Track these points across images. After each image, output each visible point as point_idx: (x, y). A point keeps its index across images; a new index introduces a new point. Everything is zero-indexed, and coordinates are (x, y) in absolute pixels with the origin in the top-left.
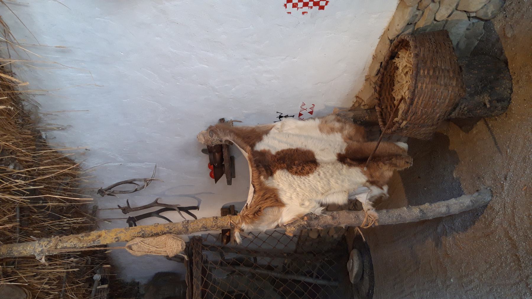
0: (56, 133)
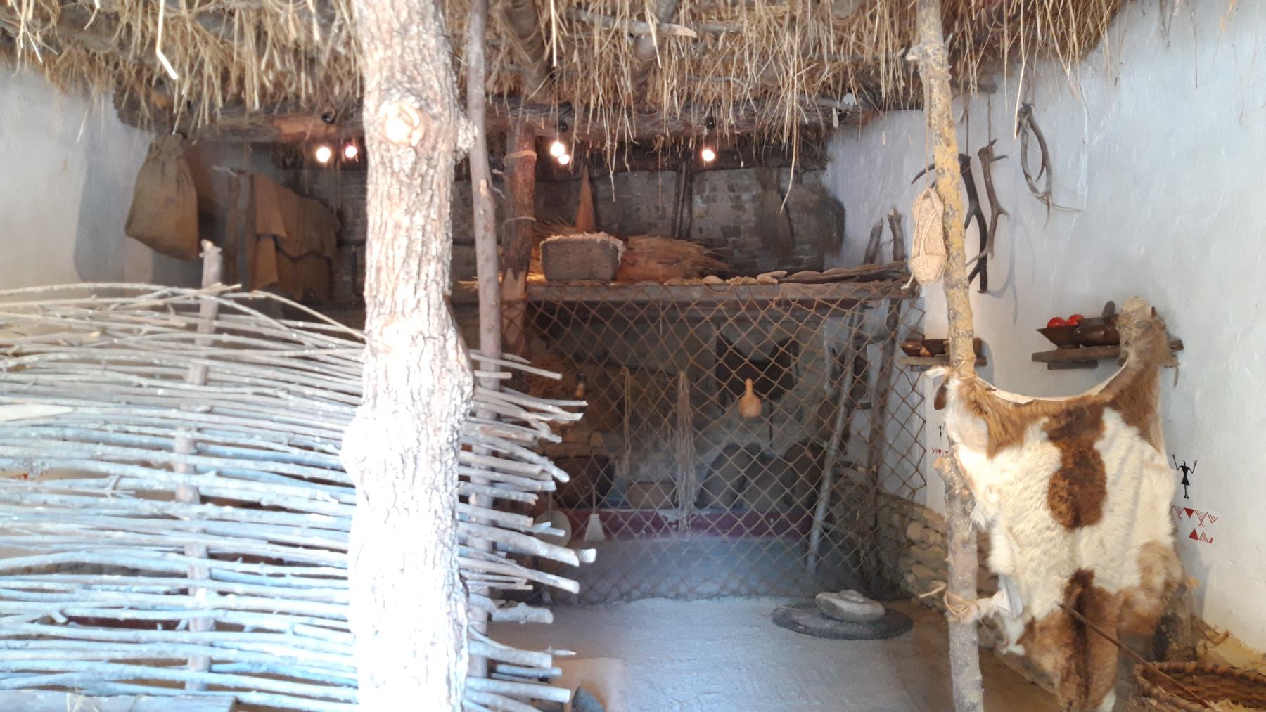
0: (1155, 25)
